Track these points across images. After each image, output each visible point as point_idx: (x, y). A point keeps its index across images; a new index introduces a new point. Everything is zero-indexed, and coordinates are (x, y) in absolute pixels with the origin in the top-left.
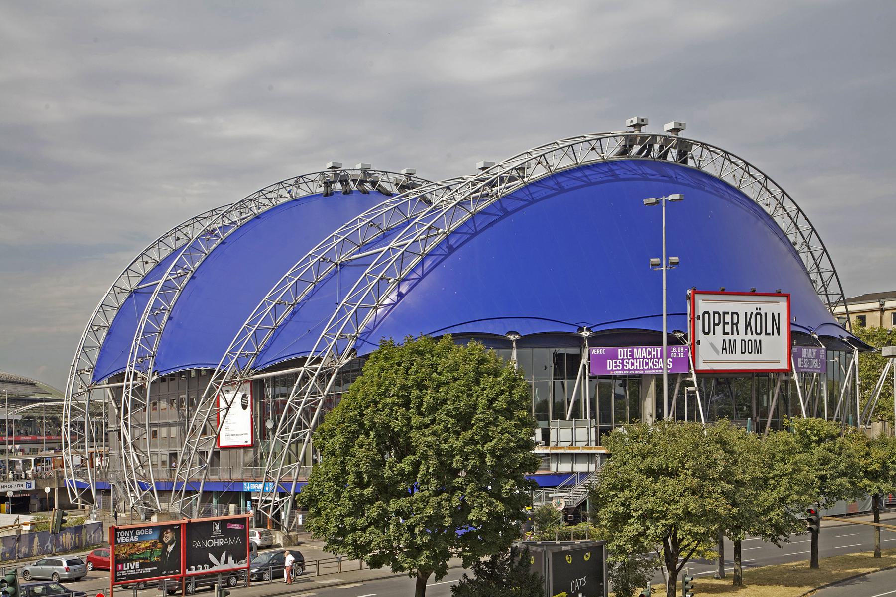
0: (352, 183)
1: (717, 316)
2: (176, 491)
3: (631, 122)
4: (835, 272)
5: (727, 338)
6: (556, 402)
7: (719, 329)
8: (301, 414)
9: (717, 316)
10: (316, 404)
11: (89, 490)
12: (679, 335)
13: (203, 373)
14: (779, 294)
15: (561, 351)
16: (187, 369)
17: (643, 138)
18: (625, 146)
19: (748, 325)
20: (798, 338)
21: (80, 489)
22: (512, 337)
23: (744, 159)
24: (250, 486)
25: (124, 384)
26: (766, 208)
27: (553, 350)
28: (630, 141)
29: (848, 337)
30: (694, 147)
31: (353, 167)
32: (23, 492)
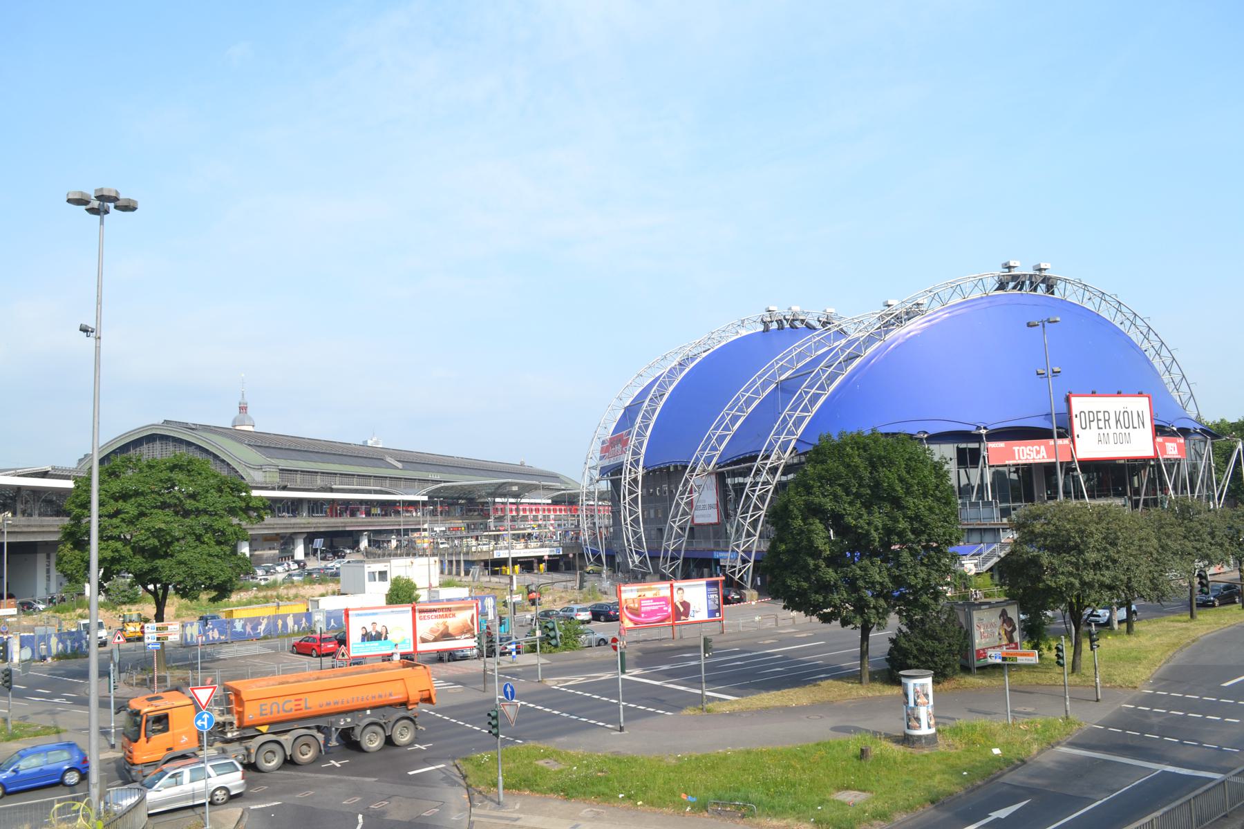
1: (1091, 414)
2: (663, 558)
5: (1101, 432)
6: (962, 486)
7: (1094, 424)
9: (1091, 414)
10: (768, 491)
11: (600, 555)
13: (680, 468)
14: (1140, 394)
15: (963, 446)
19: (1118, 421)
20: (1159, 430)
21: (593, 555)
26: (1121, 327)
27: (956, 445)
29: (1200, 429)
30: (1059, 282)
31: (780, 310)
32: (555, 556)
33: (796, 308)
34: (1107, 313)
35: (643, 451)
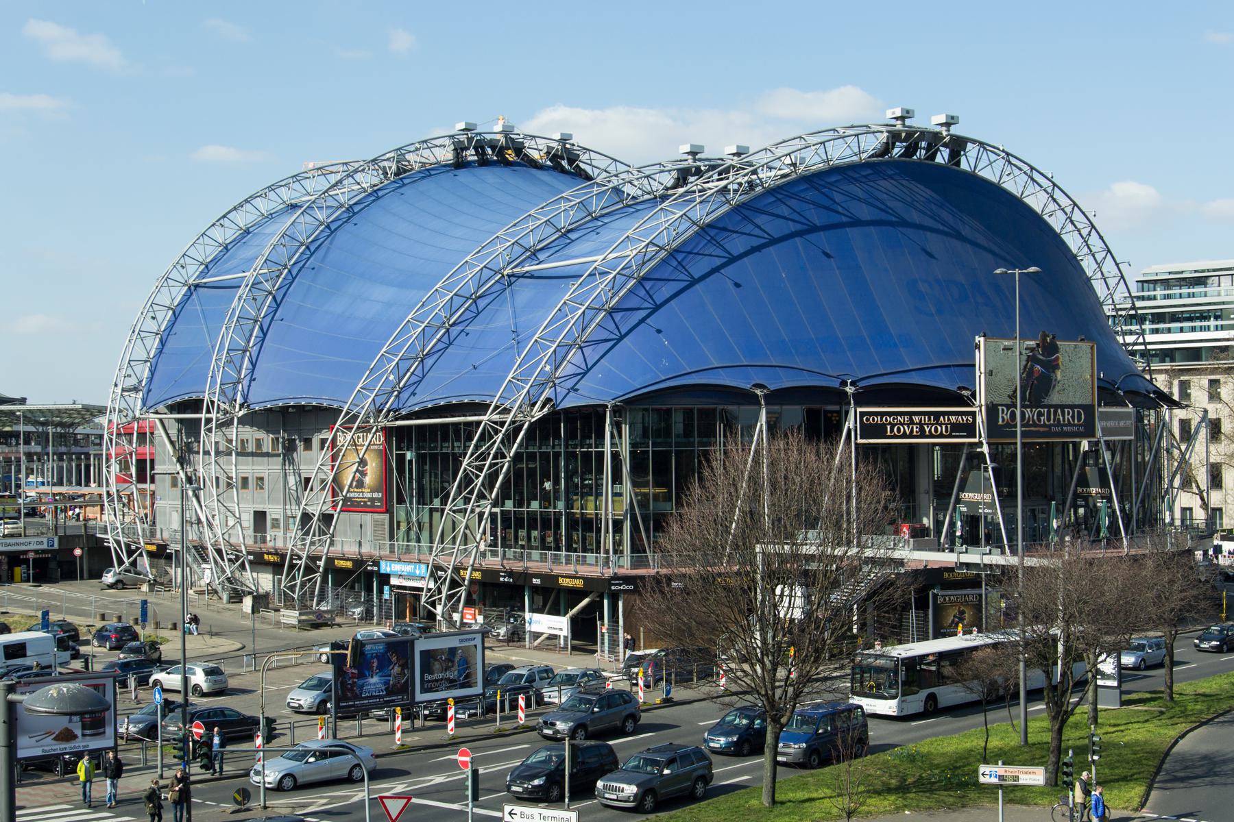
3: (894, 113)
4: (1122, 277)
8: (483, 484)
12: (965, 393)
17: (910, 134)
18: (887, 143)
22: (758, 392)
23: (1028, 162)
24: (390, 566)
25: (203, 416)
28: (894, 137)
31: (493, 129)
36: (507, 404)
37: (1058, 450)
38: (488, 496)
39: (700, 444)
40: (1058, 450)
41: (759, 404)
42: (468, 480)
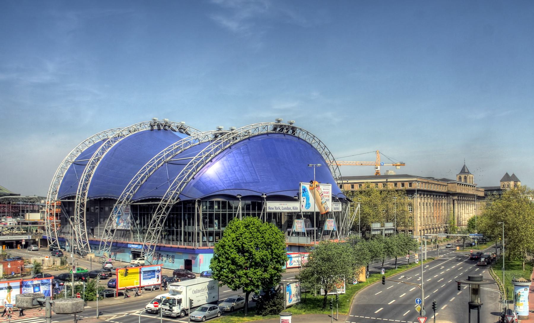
0: (161, 126)
16: (115, 199)
17: (281, 126)
30: (298, 129)
33: (167, 120)
34: (315, 145)
35: (88, 188)
36: (166, 199)
37: (226, 210)
38: (160, 225)
39: (234, 211)
40: (226, 210)
41: (239, 200)
42: (155, 221)
